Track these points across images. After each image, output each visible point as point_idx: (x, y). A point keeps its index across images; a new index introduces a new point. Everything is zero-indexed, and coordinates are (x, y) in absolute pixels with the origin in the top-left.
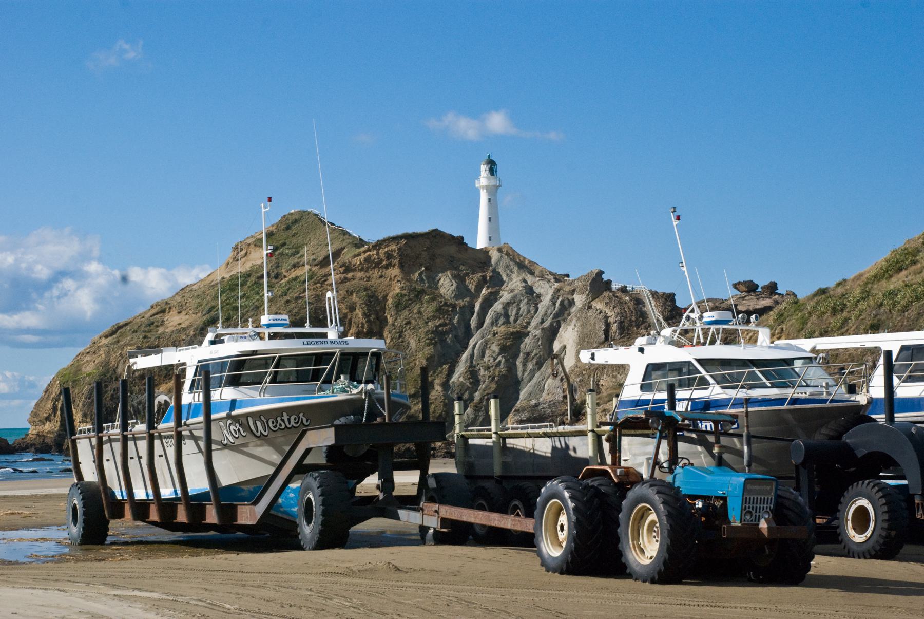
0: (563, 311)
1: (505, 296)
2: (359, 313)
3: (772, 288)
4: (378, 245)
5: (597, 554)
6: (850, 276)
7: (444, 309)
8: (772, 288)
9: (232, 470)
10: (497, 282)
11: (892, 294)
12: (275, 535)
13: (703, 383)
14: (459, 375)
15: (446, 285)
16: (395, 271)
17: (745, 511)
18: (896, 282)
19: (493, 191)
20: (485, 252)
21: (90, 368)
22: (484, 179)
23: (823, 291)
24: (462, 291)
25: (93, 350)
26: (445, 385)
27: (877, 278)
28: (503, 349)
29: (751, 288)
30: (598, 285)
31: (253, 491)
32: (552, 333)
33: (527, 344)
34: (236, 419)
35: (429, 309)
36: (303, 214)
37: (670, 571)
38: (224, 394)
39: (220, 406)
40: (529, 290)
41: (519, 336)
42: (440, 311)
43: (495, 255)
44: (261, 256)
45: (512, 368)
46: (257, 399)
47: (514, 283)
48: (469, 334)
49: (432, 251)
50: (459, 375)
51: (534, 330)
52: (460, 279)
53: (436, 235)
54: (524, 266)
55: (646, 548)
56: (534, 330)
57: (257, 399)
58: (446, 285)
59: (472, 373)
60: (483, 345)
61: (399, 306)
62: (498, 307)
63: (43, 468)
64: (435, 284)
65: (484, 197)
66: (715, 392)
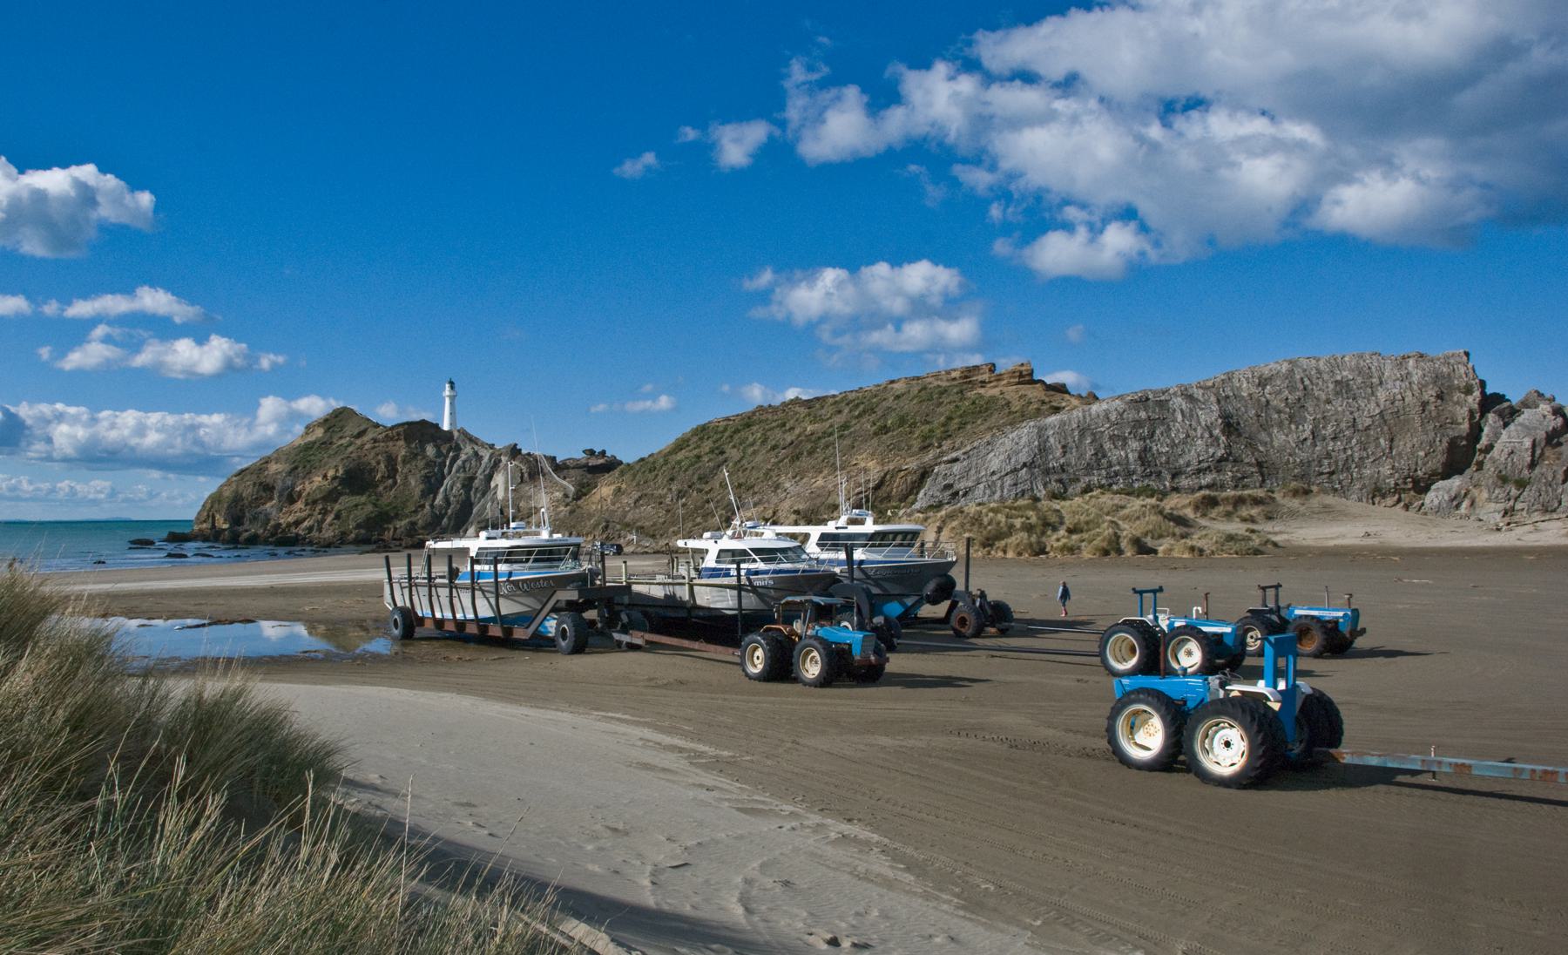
0: (495, 465)
1: (463, 457)
2: (382, 465)
3: (603, 453)
4: (392, 428)
5: (782, 669)
6: (655, 451)
7: (429, 464)
8: (603, 453)
9: (508, 608)
10: (458, 449)
11: (679, 462)
12: (541, 643)
13: (754, 561)
14: (439, 500)
15: (430, 450)
16: (401, 443)
17: (863, 650)
18: (680, 456)
19: (452, 398)
20: (450, 433)
21: (227, 493)
22: (447, 391)
23: (642, 460)
24: (439, 454)
25: (228, 483)
26: (432, 506)
27: (670, 453)
28: (463, 486)
29: (591, 452)
30: (514, 452)
31: (524, 619)
32: (490, 477)
33: (476, 483)
34: (515, 583)
35: (421, 464)
36: (344, 409)
37: (825, 681)
38: (502, 567)
39: (503, 575)
40: (476, 454)
41: (472, 479)
42: (428, 465)
43: (456, 434)
44: (319, 432)
45: (468, 497)
46: (524, 573)
47: (467, 450)
48: (444, 478)
49: (421, 432)
50: (439, 500)
51: (480, 476)
52: (438, 447)
53: (423, 422)
54: (473, 440)
55: (812, 669)
56: (480, 476)
57: (524, 573)
58: (430, 450)
59: (447, 499)
60: (451, 484)
61: (404, 462)
62: (459, 462)
63: (225, 554)
64: (424, 450)
65: (447, 401)
66: (761, 566)
